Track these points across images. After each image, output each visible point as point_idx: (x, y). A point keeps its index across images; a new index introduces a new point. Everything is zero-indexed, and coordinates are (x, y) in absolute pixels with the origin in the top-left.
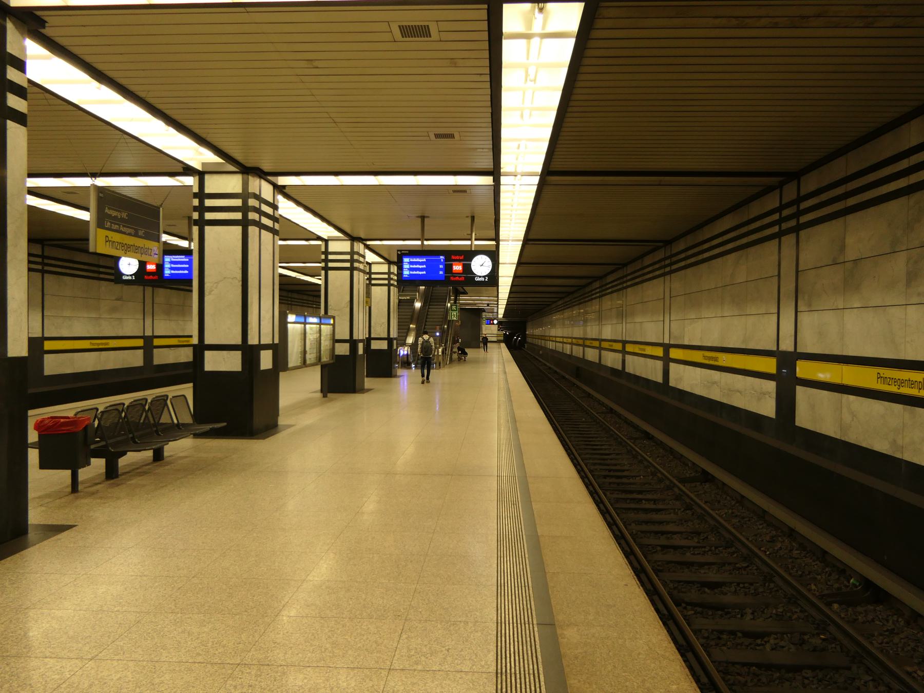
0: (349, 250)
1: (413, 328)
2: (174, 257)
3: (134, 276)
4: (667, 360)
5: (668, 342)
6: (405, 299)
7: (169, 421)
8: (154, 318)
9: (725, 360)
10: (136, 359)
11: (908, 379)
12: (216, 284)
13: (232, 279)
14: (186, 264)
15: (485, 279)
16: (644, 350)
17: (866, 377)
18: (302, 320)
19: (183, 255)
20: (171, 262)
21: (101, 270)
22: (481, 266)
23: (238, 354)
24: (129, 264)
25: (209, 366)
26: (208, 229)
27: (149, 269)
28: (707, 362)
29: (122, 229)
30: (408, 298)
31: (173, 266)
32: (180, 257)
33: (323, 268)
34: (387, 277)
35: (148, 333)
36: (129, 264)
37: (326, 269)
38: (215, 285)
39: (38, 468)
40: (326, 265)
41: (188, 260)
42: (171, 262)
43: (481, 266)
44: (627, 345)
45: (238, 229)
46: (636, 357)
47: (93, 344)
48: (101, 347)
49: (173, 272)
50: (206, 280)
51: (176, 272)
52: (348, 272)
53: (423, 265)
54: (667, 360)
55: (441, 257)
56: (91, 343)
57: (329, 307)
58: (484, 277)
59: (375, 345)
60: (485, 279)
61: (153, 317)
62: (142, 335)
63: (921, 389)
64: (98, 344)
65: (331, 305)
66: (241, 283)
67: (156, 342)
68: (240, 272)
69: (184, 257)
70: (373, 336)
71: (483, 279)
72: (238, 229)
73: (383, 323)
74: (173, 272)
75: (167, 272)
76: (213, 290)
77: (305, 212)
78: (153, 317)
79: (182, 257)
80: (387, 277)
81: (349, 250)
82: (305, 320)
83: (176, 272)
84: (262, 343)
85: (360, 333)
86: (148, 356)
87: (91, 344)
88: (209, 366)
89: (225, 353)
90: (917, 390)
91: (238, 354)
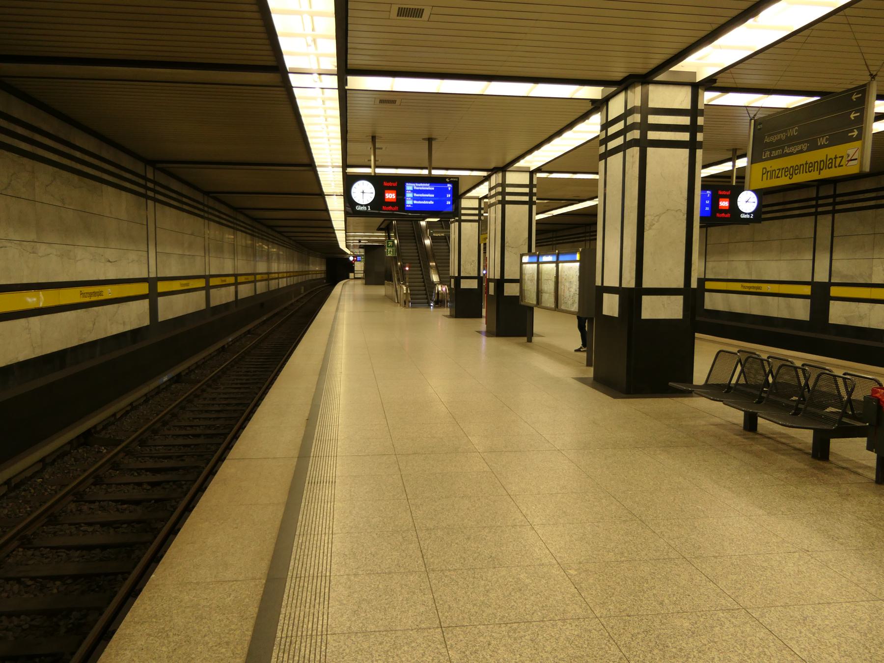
0: (528, 182)
1: (432, 262)
2: (417, 184)
3: (369, 207)
4: (207, 288)
5: (493, 278)
6: (439, 236)
7: (794, 382)
8: (834, 257)
9: (72, 296)
10: (801, 311)
11: (804, 162)
12: (658, 217)
13: (677, 211)
14: (431, 194)
15: (750, 216)
16: (246, 279)
17: (109, 292)
18: (535, 260)
19: (428, 183)
20: (414, 191)
21: (184, 200)
22: (747, 202)
23: (680, 299)
24: (363, 192)
25: (647, 314)
26: (650, 151)
27: (726, 201)
28: (87, 299)
29: (787, 151)
30: (443, 235)
31: (415, 195)
32: (424, 185)
33: (499, 202)
34: (478, 213)
35: (822, 277)
36: (363, 192)
37: (504, 203)
38: (656, 218)
39: (865, 448)
40: (504, 198)
41: (433, 189)
42: (414, 191)
43: (747, 202)
44: (239, 278)
45: (685, 153)
46: (749, 296)
47: (744, 287)
48: (752, 290)
49: (415, 202)
50: (647, 212)
51: (420, 202)
52: (527, 207)
53: (429, 200)
54: (153, 296)
55: (708, 192)
56: (742, 286)
57: (506, 245)
58: (750, 214)
59: (465, 284)
60: (750, 216)
61: (156, 247)
62: (810, 280)
63: (822, 170)
64: (750, 287)
65: (508, 242)
66: (686, 216)
67: (162, 287)
68: (685, 203)
69: (429, 185)
70: (462, 275)
71: (748, 216)
72: (685, 153)
73: (473, 261)
74: (415, 202)
75: (409, 202)
76: (654, 224)
77: (561, 137)
78: (156, 247)
79: (426, 185)
80: (478, 213)
81: (528, 182)
82: (538, 260)
83: (420, 202)
84: (706, 277)
85: (493, 272)
86: (153, 310)
87: (182, 285)
88: (647, 314)
89: (664, 298)
90: (817, 173)
91: (680, 299)
